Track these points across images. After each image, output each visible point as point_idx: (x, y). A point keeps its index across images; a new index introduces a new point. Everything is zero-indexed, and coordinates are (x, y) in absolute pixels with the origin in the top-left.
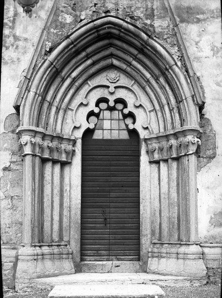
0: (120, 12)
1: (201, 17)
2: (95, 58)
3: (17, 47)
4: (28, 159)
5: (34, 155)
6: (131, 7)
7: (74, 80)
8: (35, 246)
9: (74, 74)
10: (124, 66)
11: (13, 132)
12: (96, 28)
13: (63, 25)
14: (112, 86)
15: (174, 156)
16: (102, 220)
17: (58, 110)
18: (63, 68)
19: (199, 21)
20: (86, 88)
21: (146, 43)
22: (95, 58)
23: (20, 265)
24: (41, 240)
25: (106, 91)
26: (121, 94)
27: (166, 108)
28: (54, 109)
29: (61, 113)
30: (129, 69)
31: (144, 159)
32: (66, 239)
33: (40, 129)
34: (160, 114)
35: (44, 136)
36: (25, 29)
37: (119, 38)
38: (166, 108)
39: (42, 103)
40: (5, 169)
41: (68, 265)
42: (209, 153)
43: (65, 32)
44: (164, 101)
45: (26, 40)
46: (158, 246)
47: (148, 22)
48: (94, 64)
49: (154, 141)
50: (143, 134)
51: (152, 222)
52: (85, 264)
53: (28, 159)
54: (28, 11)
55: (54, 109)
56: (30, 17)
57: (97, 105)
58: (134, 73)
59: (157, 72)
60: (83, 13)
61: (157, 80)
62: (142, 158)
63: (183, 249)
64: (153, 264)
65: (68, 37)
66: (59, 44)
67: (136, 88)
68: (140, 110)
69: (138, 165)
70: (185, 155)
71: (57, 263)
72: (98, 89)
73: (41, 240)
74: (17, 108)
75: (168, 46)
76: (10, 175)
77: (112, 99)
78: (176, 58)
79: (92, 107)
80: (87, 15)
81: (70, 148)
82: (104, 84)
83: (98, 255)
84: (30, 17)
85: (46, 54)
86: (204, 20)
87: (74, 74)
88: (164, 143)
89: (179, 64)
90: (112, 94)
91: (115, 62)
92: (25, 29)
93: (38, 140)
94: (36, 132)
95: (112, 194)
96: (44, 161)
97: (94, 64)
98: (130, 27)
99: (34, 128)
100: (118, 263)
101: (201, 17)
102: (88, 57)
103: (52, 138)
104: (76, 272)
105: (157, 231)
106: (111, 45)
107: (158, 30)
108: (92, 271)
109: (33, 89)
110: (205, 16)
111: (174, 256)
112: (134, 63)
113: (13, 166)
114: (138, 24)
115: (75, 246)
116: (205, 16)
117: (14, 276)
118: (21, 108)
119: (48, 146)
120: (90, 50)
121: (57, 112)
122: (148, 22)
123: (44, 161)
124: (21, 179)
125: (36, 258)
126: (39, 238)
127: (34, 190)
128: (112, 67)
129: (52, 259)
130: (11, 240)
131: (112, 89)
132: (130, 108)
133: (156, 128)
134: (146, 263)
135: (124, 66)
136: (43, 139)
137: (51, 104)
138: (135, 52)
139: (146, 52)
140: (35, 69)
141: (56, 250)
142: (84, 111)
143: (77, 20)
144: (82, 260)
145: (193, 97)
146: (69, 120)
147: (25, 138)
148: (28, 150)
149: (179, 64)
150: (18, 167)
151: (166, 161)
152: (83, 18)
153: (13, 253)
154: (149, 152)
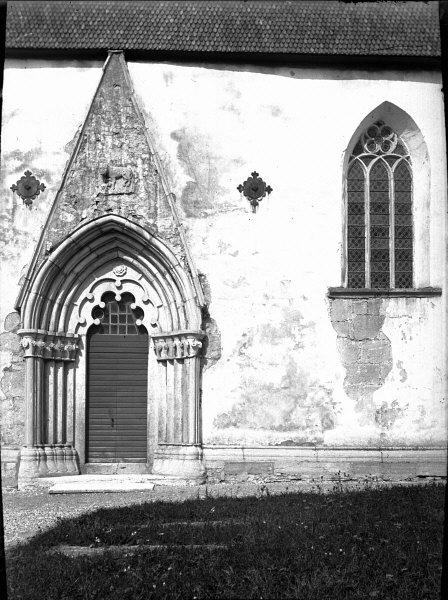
0: (123, 210)
1: (209, 211)
2: (100, 252)
3: (16, 242)
4: (29, 361)
6: (133, 206)
7: (78, 275)
8: (37, 447)
9: (77, 270)
11: (14, 331)
12: (98, 226)
13: (64, 225)
14: (119, 279)
15: (179, 357)
16: (439, 452)
18: (65, 265)
19: (206, 215)
20: (76, 309)
24: (44, 441)
27: (173, 306)
31: (152, 357)
32: (69, 439)
35: (46, 338)
36: (25, 222)
37: (123, 234)
40: (6, 370)
41: (70, 466)
42: (214, 354)
43: (66, 231)
45: (26, 234)
46: (163, 447)
47: (151, 221)
48: (98, 257)
50: (152, 332)
51: (160, 423)
54: (28, 203)
56: (30, 209)
57: (103, 299)
60: (85, 211)
61: (163, 276)
62: (150, 356)
64: (158, 465)
65: (69, 236)
66: (60, 243)
67: (143, 282)
73: (44, 441)
74: (18, 309)
75: (171, 246)
76: (12, 376)
78: (179, 258)
80: (88, 213)
83: (104, 457)
84: (30, 209)
85: (46, 254)
86: (212, 215)
87: (77, 270)
88: (169, 342)
89: (182, 264)
92: (25, 222)
93: (40, 343)
95: (119, 394)
96: (46, 362)
97: (98, 257)
98: (134, 226)
100: (122, 464)
101: (209, 211)
102: (92, 251)
105: (164, 432)
106: (116, 239)
107: (160, 230)
109: (34, 290)
110: (213, 211)
113: (14, 367)
114: (141, 223)
115: (79, 448)
116: (213, 211)
117: (17, 474)
118: (22, 310)
122: (151, 221)
123: (46, 362)
124: (23, 380)
126: (41, 437)
127: (35, 392)
130: (13, 441)
132: (138, 303)
133: (166, 327)
134: (151, 465)
138: (141, 248)
139: (149, 250)
140: (33, 268)
141: (58, 451)
142: (89, 307)
143: (79, 219)
144: (87, 461)
148: (29, 353)
149: (182, 264)
150: (20, 368)
151: (172, 361)
152: (84, 216)
153: (16, 453)
154: (158, 351)
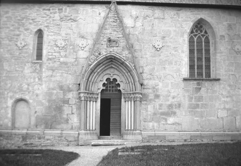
2: (106, 65)
5: (85, 100)
7: (98, 73)
8: (85, 130)
10: (116, 68)
17: (93, 83)
21: (124, 62)
22: (106, 65)
23: (80, 136)
25: (110, 75)
26: (115, 77)
28: (91, 83)
29: (94, 84)
30: (118, 69)
31: (123, 100)
33: (87, 92)
34: (128, 85)
35: (88, 93)
37: (114, 59)
38: (131, 83)
39: (87, 82)
44: (130, 81)
48: (105, 67)
49: (126, 94)
50: (122, 91)
52: (102, 137)
53: (83, 102)
55: (91, 83)
57: (106, 81)
58: (120, 70)
59: (127, 71)
61: (127, 73)
62: (122, 100)
63: (134, 132)
68: (122, 82)
69: (121, 104)
70: (136, 101)
71: (87, 136)
72: (107, 75)
75: (131, 64)
77: (112, 79)
79: (105, 81)
81: (96, 96)
82: (109, 73)
90: (112, 77)
91: (113, 66)
94: (85, 93)
97: (105, 67)
99: (85, 91)
102: (103, 65)
103: (91, 94)
104: (98, 139)
108: (51, 130)
111: (131, 134)
112: (120, 67)
119: (89, 97)
120: (104, 63)
121: (92, 84)
125: (85, 134)
128: (112, 67)
129: (91, 135)
131: (112, 75)
135: (116, 68)
136: (88, 94)
137: (90, 82)
138: (120, 64)
145: (139, 81)
146: (96, 86)
147: (82, 95)
148: (83, 99)
